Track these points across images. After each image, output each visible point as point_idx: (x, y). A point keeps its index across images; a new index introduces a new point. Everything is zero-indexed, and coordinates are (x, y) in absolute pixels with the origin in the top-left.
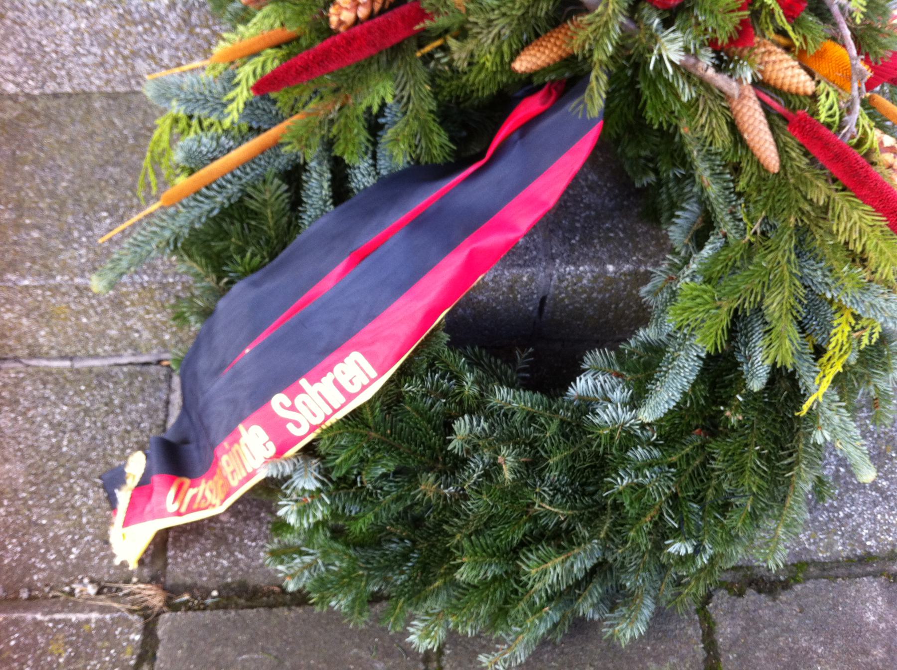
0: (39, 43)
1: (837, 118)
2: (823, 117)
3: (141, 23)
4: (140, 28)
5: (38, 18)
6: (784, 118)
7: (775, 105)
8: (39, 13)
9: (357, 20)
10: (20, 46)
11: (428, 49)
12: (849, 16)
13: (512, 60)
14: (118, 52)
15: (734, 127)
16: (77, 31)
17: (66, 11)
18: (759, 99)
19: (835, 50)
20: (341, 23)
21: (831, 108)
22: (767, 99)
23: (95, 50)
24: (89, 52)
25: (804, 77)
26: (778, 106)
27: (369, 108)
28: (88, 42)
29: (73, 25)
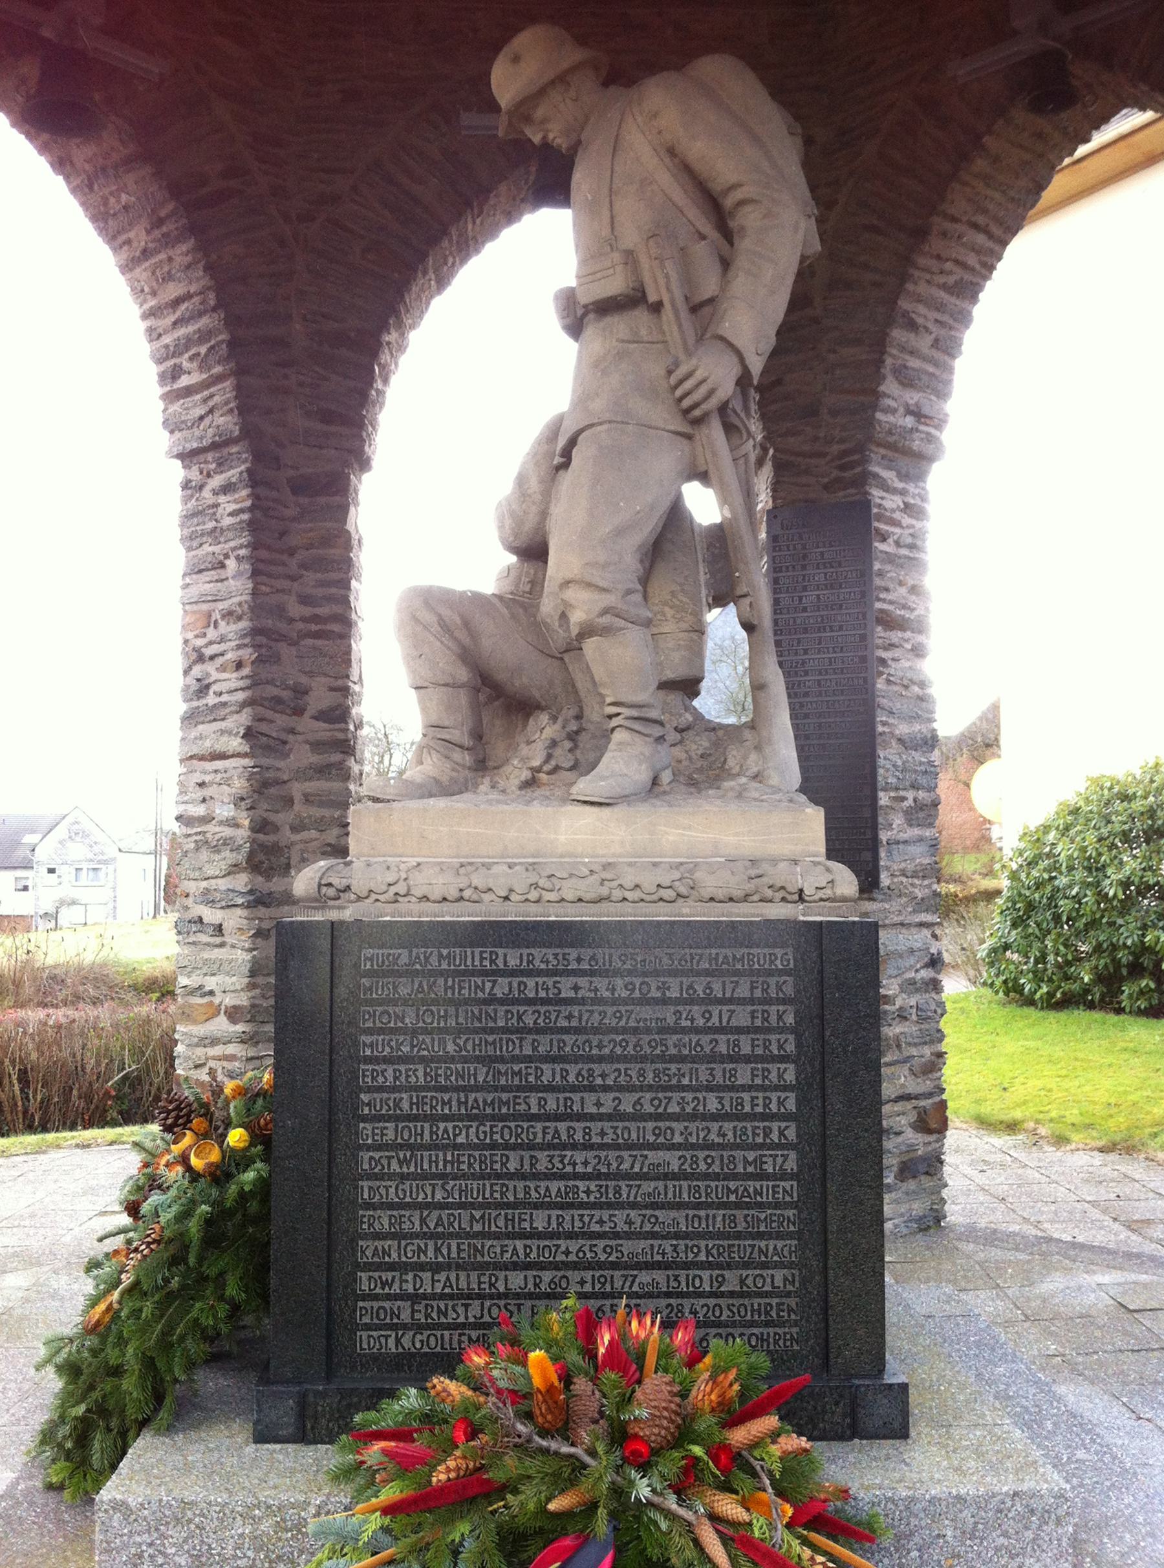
0: (209, 1546)
1: (767, 1534)
2: (757, 1534)
3: (291, 1530)
4: (289, 1535)
5: (216, 1523)
6: (732, 1539)
7: (726, 1531)
8: (218, 1518)
9: (449, 1479)
10: (194, 1549)
11: (495, 1506)
12: (770, 1474)
13: (547, 1504)
14: (266, 1557)
15: (697, 1542)
16: (241, 1535)
17: (239, 1518)
18: (717, 1531)
19: (762, 1495)
20: (439, 1481)
21: (761, 1528)
22: (720, 1528)
23: (250, 1554)
24: (245, 1556)
25: (740, 1509)
26: (730, 1531)
27: (453, 1541)
28: (247, 1545)
29: (240, 1531)
